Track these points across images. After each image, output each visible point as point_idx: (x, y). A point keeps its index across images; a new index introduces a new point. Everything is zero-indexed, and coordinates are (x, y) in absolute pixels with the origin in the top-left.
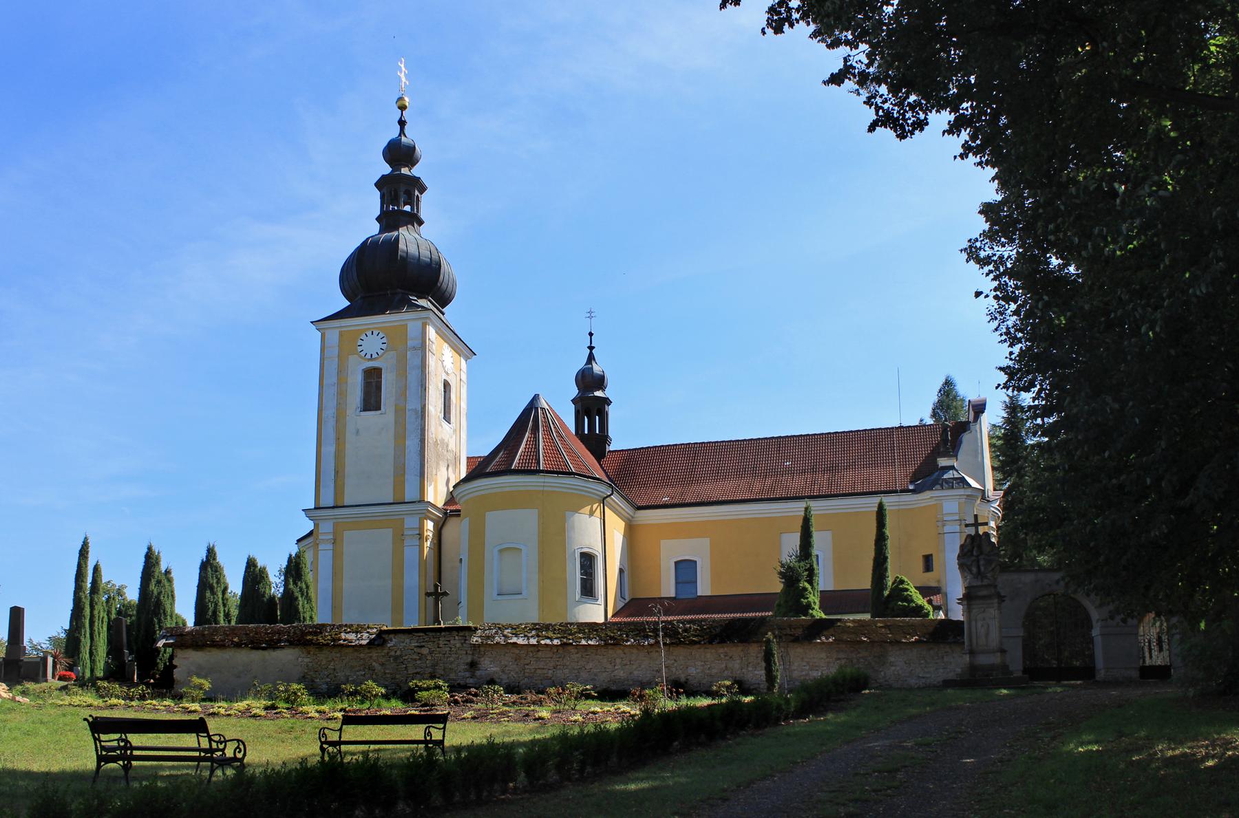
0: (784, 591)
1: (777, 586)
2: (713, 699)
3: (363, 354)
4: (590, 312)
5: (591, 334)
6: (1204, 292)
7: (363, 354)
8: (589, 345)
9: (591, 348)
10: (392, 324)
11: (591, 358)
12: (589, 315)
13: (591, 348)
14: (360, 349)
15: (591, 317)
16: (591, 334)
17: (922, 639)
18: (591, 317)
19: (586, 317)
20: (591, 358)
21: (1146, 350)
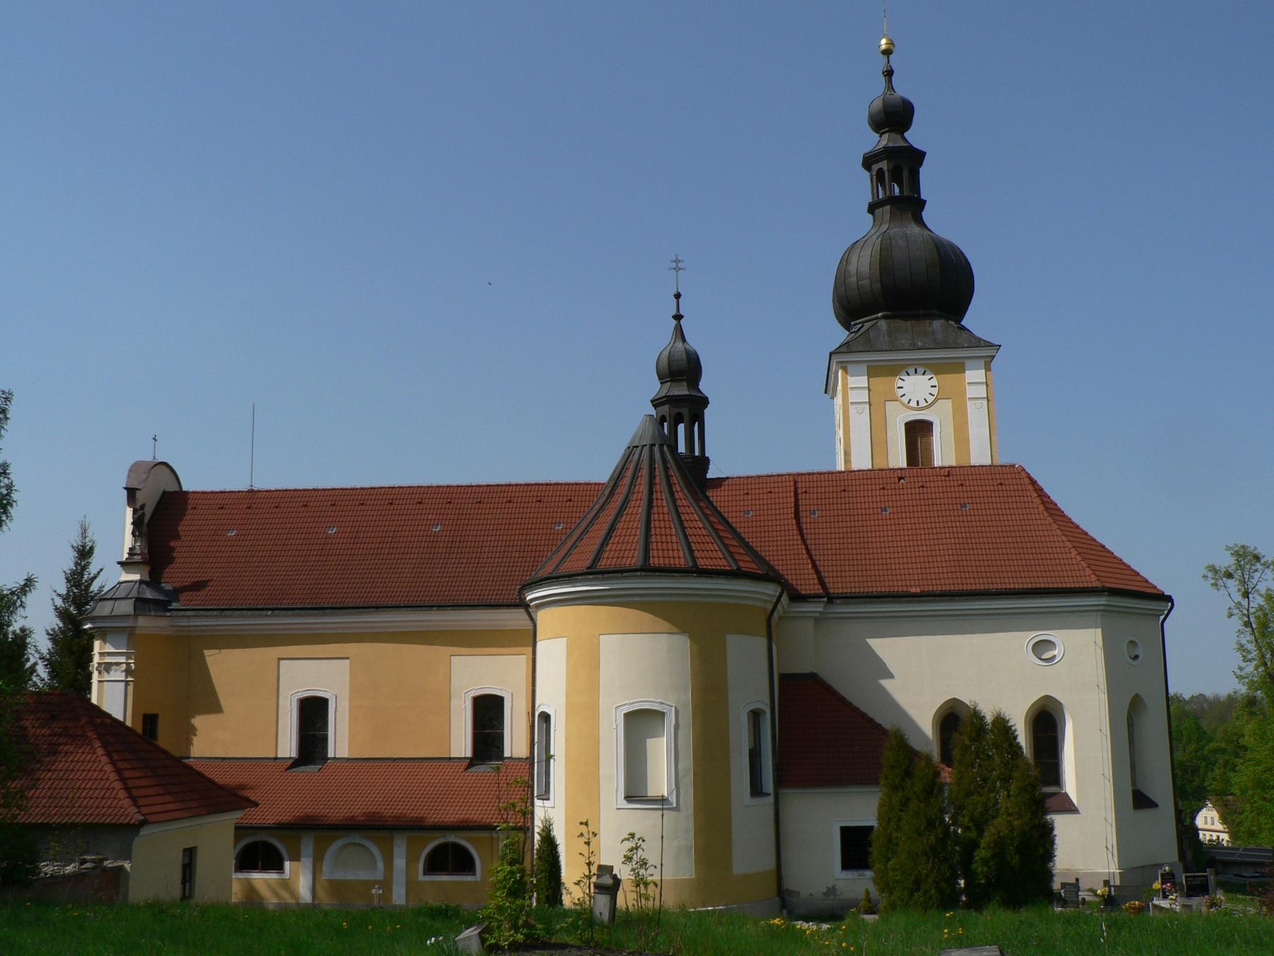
0: (66, 594)
1: (1074, 881)
2: (51, 663)
3: (905, 400)
4: (677, 261)
5: (678, 296)
6: (1179, 784)
7: (905, 400)
8: (674, 312)
9: (678, 317)
10: (888, 363)
11: (680, 333)
12: (674, 265)
13: (678, 317)
14: (901, 392)
15: (677, 269)
16: (678, 296)
17: (36, 877)
18: (677, 269)
19: (671, 269)
20: (680, 333)
21: (960, 929)
